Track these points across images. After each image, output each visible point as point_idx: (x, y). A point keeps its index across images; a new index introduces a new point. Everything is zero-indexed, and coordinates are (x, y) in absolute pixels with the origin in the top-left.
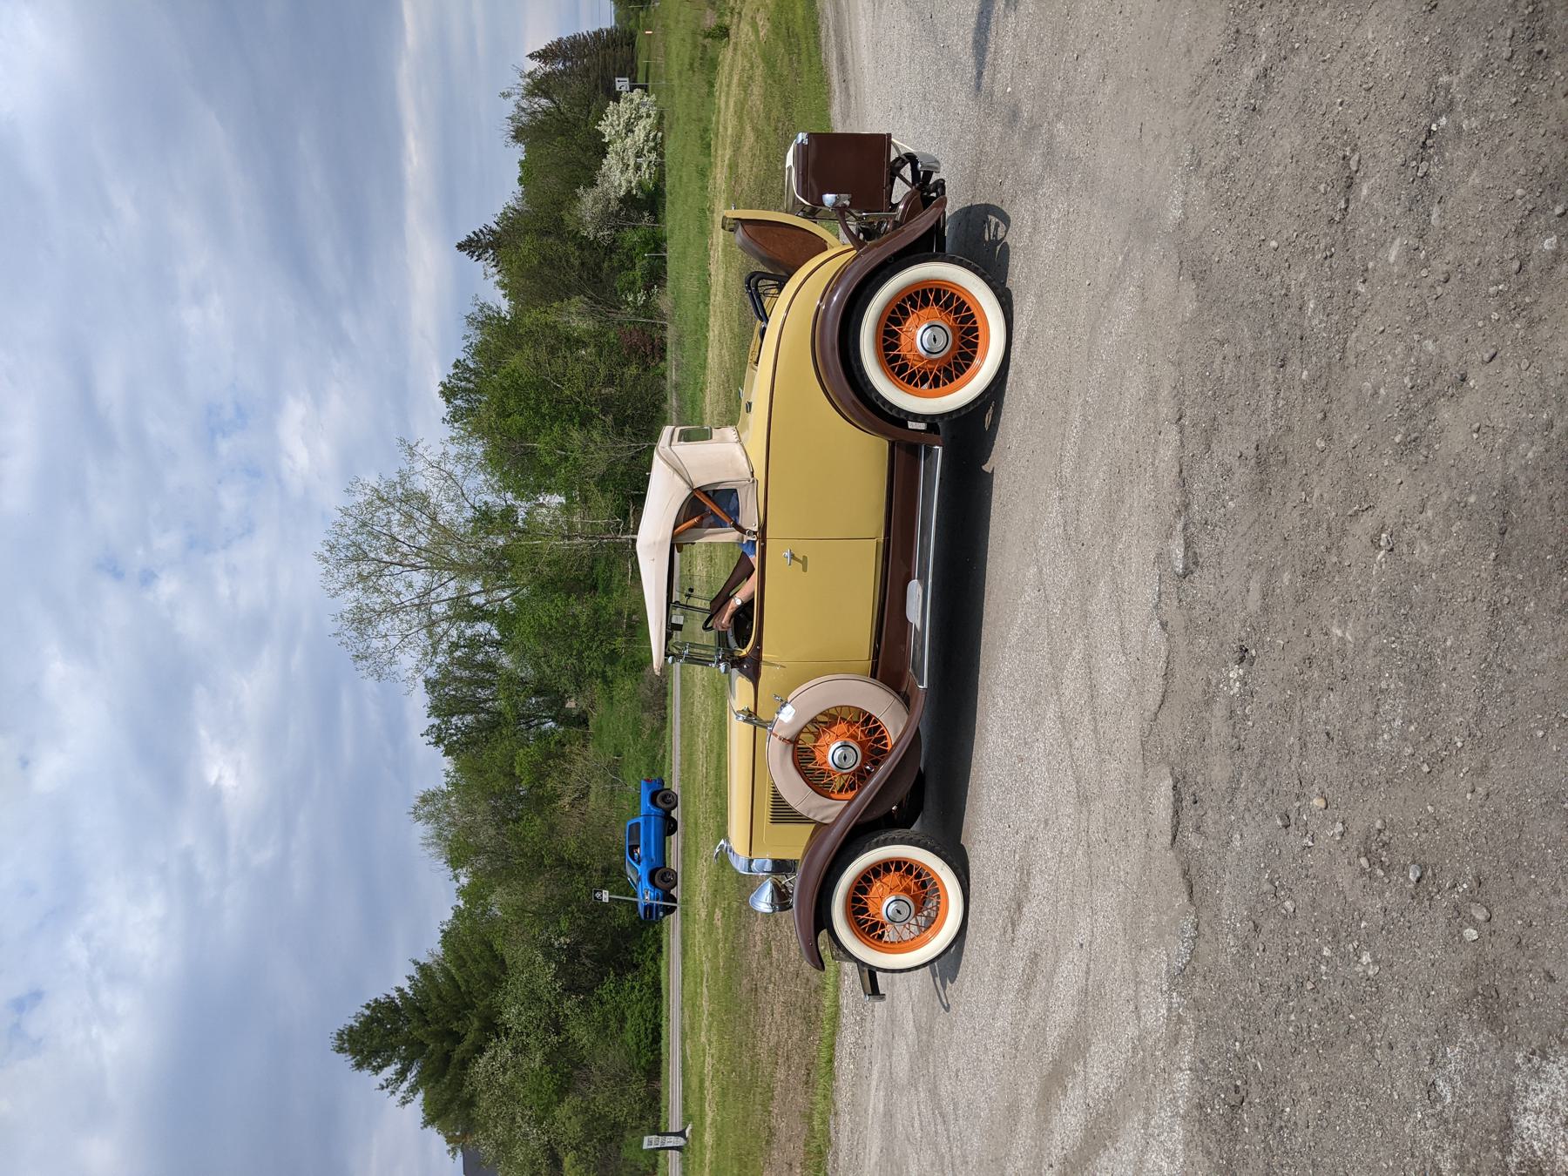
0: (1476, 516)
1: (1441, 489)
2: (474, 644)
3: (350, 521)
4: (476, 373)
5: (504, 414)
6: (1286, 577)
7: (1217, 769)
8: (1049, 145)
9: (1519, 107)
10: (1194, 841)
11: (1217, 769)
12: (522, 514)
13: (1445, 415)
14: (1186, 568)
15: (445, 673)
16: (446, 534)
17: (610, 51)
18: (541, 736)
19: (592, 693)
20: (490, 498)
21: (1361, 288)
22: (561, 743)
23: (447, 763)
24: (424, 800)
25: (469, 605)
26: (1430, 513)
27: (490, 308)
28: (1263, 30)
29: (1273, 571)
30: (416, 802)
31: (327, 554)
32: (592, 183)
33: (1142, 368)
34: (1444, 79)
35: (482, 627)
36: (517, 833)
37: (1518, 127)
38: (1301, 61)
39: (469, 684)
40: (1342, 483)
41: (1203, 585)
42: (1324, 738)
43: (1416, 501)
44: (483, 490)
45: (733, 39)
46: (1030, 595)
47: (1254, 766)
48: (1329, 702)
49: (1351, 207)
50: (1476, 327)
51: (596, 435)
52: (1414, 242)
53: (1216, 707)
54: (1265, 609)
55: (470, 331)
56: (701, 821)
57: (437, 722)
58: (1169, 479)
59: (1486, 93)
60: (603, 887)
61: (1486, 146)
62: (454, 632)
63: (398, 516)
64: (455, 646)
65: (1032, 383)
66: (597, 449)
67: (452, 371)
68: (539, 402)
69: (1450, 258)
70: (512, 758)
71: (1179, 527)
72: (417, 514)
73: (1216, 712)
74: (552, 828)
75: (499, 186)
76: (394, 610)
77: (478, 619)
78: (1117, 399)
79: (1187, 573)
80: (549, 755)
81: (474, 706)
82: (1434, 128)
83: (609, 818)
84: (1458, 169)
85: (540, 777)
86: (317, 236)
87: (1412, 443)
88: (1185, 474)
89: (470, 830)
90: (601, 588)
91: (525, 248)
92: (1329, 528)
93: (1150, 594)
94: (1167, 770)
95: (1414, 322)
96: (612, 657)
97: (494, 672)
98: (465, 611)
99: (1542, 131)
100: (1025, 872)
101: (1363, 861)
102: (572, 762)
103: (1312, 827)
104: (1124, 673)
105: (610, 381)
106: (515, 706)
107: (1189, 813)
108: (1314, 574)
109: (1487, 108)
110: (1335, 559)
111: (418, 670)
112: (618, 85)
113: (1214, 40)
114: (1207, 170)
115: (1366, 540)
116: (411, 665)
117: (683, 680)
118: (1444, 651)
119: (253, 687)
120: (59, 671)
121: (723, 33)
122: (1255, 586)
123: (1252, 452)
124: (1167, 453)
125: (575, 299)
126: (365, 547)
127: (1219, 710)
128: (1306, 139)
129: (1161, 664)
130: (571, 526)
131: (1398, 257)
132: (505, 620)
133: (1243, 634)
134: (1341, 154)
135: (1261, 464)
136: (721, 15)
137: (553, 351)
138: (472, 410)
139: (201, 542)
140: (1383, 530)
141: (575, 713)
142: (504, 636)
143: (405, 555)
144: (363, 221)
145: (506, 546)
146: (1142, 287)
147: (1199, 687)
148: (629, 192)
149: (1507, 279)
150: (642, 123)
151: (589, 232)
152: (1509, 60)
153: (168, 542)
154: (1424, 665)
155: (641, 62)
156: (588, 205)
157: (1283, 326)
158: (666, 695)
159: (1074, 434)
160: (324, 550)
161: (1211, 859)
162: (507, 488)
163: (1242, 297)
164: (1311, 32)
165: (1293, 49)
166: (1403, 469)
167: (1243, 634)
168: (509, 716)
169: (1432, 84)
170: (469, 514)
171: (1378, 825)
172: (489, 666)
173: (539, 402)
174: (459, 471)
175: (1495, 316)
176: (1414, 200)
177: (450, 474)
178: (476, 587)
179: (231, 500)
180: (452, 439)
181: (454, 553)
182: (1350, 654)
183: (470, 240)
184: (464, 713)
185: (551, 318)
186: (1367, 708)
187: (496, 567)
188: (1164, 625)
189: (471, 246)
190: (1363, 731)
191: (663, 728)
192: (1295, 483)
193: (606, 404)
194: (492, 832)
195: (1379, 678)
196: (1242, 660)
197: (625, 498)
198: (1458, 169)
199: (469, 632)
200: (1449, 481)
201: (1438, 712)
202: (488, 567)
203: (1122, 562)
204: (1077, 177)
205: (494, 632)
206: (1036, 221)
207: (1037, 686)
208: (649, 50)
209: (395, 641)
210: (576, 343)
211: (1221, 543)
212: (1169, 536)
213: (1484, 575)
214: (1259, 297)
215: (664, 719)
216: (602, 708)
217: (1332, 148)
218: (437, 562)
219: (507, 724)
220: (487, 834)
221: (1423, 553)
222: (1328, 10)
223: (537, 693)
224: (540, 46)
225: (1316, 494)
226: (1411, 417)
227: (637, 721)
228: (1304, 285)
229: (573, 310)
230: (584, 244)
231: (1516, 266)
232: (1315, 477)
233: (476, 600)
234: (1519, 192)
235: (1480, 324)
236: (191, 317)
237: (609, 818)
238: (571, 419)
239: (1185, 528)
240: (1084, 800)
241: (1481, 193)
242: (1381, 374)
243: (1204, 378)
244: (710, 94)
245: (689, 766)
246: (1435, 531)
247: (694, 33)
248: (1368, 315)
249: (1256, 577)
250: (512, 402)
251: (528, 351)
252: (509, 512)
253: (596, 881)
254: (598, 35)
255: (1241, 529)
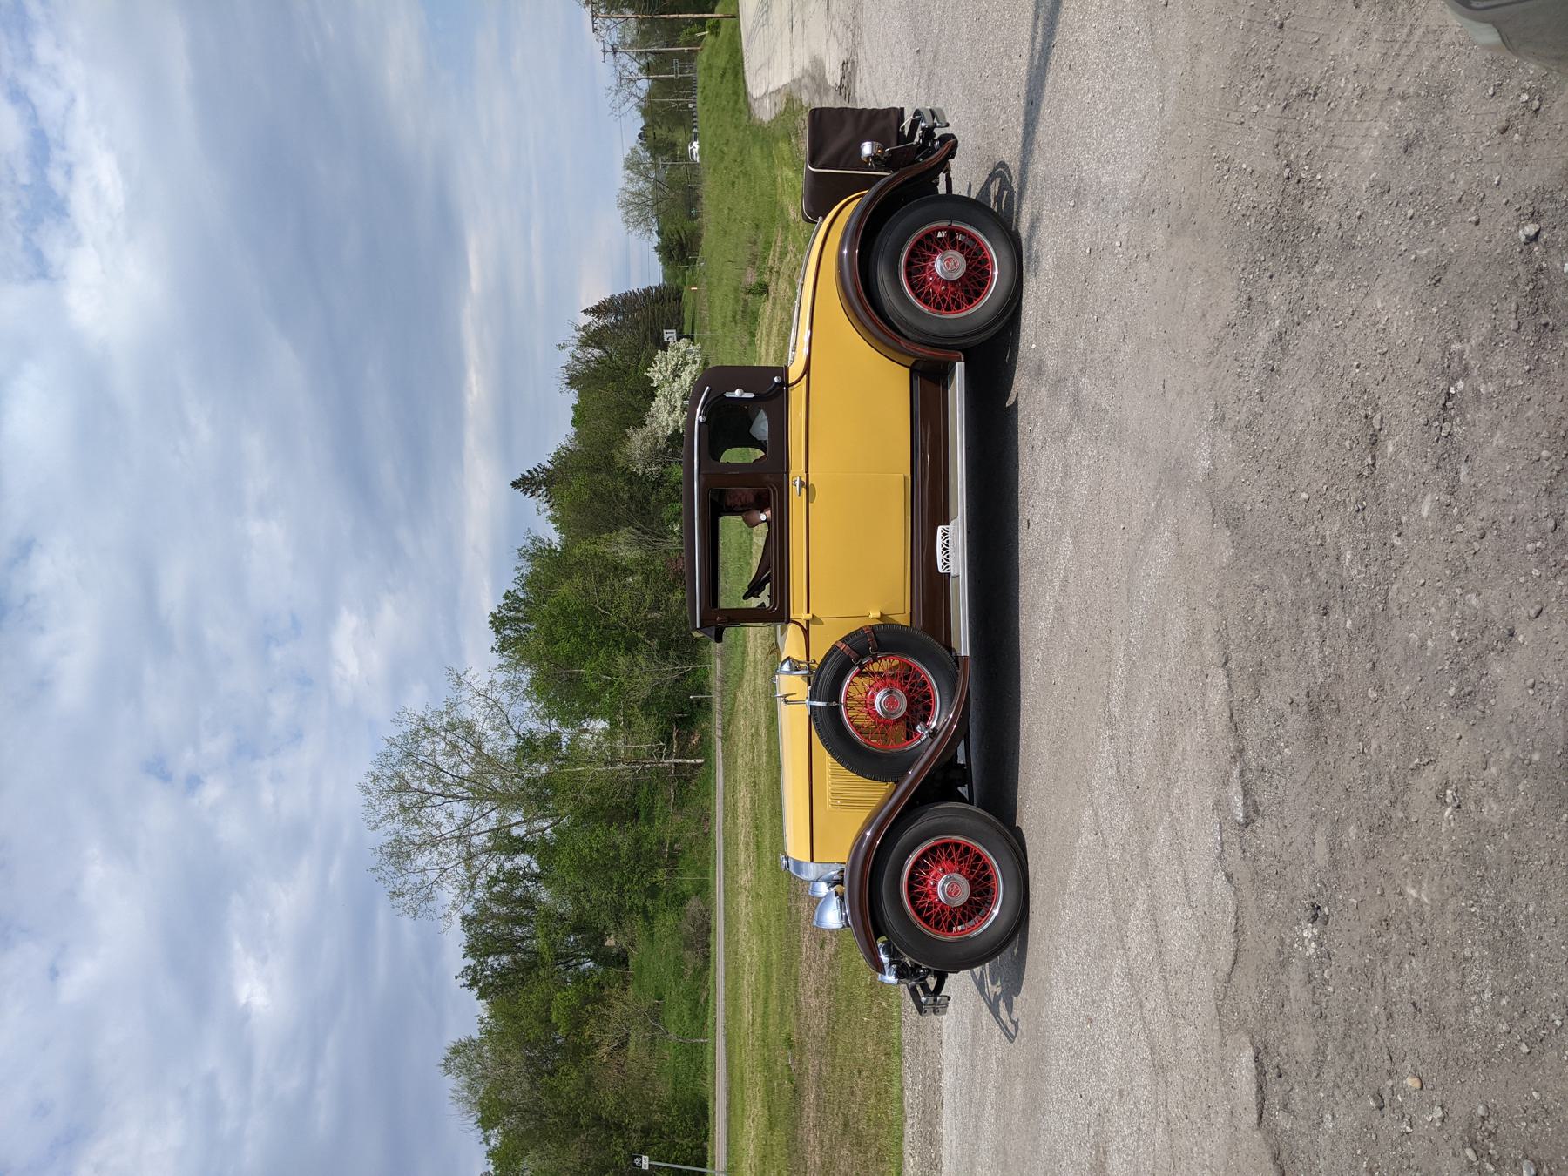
0: (1543, 774)
1: (1503, 745)
2: (513, 877)
3: (396, 750)
4: (526, 602)
5: (552, 641)
6: (1352, 831)
7: (1300, 1039)
8: (1076, 398)
9: (1533, 374)
10: (1282, 1120)
11: (1300, 1039)
12: (565, 739)
13: (1497, 669)
14: (1246, 816)
15: (483, 908)
16: (489, 762)
17: (659, 306)
18: (580, 978)
19: (632, 928)
20: (534, 725)
21: (1397, 541)
22: (599, 985)
23: (481, 1008)
24: (456, 1051)
25: (510, 837)
26: (1494, 770)
27: (541, 541)
28: (1274, 298)
29: (1338, 824)
30: (447, 1053)
31: (371, 785)
32: (642, 424)
33: (1184, 610)
34: (1456, 346)
35: (522, 860)
36: (553, 1088)
37: (1535, 391)
38: (1314, 327)
39: (507, 922)
40: (1400, 735)
41: (1265, 835)
42: (1411, 1009)
43: (1478, 757)
44: (528, 717)
45: (772, 295)
46: (1087, 838)
47: (1339, 1037)
48: (1411, 969)
49: (1379, 463)
50: (1518, 583)
51: (641, 660)
52: (1445, 498)
53: (1292, 969)
54: (1335, 864)
55: (522, 563)
56: (747, 1074)
57: (472, 962)
58: (1220, 725)
59: (1498, 361)
60: (642, 1152)
61: (1506, 409)
62: (493, 866)
63: (443, 745)
64: (494, 881)
65: (1073, 621)
66: (643, 674)
67: (502, 602)
68: (587, 628)
69: (1483, 514)
70: (549, 1002)
71: (1236, 773)
72: (461, 743)
73: (1292, 975)
74: (589, 1081)
75: (553, 428)
76: (434, 843)
77: (517, 852)
78: (1160, 640)
79: (1248, 822)
80: (587, 1000)
81: (508, 945)
82: (1452, 390)
83: (649, 1069)
84: (1480, 430)
85: (577, 1024)
86: (378, 466)
87: (1466, 698)
88: (1236, 718)
89: (505, 1084)
90: (642, 815)
91: (576, 485)
92: (1391, 781)
93: (1211, 842)
94: (1246, 1039)
95: (1455, 576)
96: (653, 891)
97: (533, 908)
98: (506, 843)
99: (1559, 397)
100: (1101, 1150)
101: (1469, 1153)
102: (611, 1007)
103: (1409, 1110)
104: (1191, 927)
105: (656, 607)
106: (553, 944)
107: (1275, 1089)
108: (1380, 828)
109: (1502, 374)
110: (1401, 815)
111: (455, 906)
112: (666, 337)
113: (1228, 305)
114: (1231, 425)
115: (1431, 795)
116: (451, 902)
117: (727, 917)
118: (1527, 917)
119: (288, 900)
120: (98, 873)
121: (763, 289)
122: (1320, 839)
123: (1302, 699)
124: (1216, 697)
125: (623, 531)
126: (408, 777)
127: (1296, 972)
128: (1326, 398)
129: (1230, 920)
130: (614, 751)
131: (1431, 512)
132: (545, 852)
133: (1314, 890)
134: (1363, 413)
135: (1314, 711)
136: (761, 274)
137: (601, 579)
138: (521, 638)
139: (248, 749)
140: (1447, 786)
141: (615, 951)
142: (543, 869)
143: (446, 785)
144: (425, 449)
145: (549, 774)
146: (1176, 533)
147: (1272, 947)
148: (676, 431)
149: (1543, 537)
150: (688, 369)
151: (638, 468)
152: (1517, 330)
153: (216, 746)
154: (1509, 932)
155: (687, 315)
156: (637, 443)
157: (1322, 575)
158: (709, 931)
159: (1119, 673)
160: (368, 781)
161: (1302, 1142)
162: (549, 716)
163: (1277, 545)
164: (1322, 301)
165: (1305, 316)
166: (1461, 724)
167: (1314, 890)
168: (546, 957)
169: (1446, 347)
170: (512, 741)
171: (1481, 1111)
172: (527, 902)
173: (587, 628)
174: (505, 699)
175: (1536, 573)
176: (1441, 458)
177: (496, 703)
178: (517, 817)
179: (281, 707)
180: (500, 666)
181: (497, 783)
182: (1428, 916)
183: (524, 478)
184: (500, 953)
185: (600, 549)
186: (1453, 976)
187: (538, 796)
188: (1229, 877)
189: (525, 484)
190: (1452, 1001)
191: (706, 967)
192: (1351, 733)
193: (652, 629)
194: (526, 1086)
195: (1461, 945)
196: (1315, 918)
197: (669, 721)
198: (1480, 430)
199: (508, 866)
200: (1509, 737)
201: (1529, 985)
202: (529, 797)
203: (1180, 808)
204: (1105, 427)
205: (534, 865)
206: (1067, 467)
207: (1102, 938)
208: (695, 305)
209: (433, 876)
210: (621, 571)
211: (1280, 791)
212: (1226, 782)
213: (1558, 837)
214: (1295, 546)
215: (707, 958)
216: (642, 946)
217: (1354, 408)
218: (480, 793)
219: (544, 964)
220: (521, 1091)
221: (1491, 811)
222: (1335, 282)
223: (576, 929)
224: (594, 302)
225: (1374, 745)
226: (1462, 670)
227: (679, 961)
228: (1338, 536)
229: (621, 540)
230: (632, 479)
231: (1551, 524)
232: (1370, 727)
233: (516, 831)
234: (1545, 453)
235: (1522, 579)
236: (256, 528)
237: (649, 1069)
238: (617, 644)
239: (1242, 774)
240: (1159, 1069)
241: (1506, 453)
242: (1425, 626)
243: (1247, 623)
244: (752, 343)
245: (734, 1011)
246: (1501, 788)
247: (736, 290)
248: (1407, 567)
249: (1321, 829)
250: (560, 630)
251: (577, 580)
252: (554, 738)
253: (636, 1143)
254: (647, 291)
255: (1300, 778)
